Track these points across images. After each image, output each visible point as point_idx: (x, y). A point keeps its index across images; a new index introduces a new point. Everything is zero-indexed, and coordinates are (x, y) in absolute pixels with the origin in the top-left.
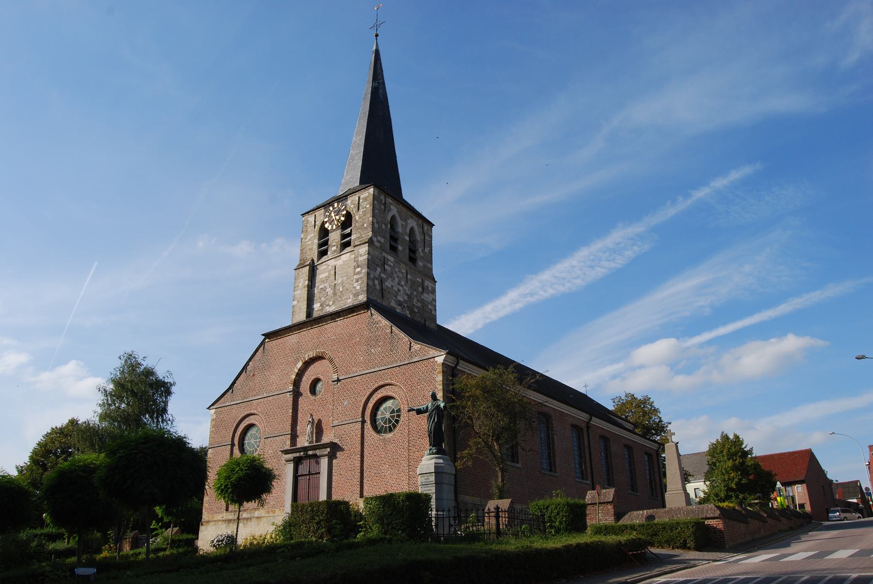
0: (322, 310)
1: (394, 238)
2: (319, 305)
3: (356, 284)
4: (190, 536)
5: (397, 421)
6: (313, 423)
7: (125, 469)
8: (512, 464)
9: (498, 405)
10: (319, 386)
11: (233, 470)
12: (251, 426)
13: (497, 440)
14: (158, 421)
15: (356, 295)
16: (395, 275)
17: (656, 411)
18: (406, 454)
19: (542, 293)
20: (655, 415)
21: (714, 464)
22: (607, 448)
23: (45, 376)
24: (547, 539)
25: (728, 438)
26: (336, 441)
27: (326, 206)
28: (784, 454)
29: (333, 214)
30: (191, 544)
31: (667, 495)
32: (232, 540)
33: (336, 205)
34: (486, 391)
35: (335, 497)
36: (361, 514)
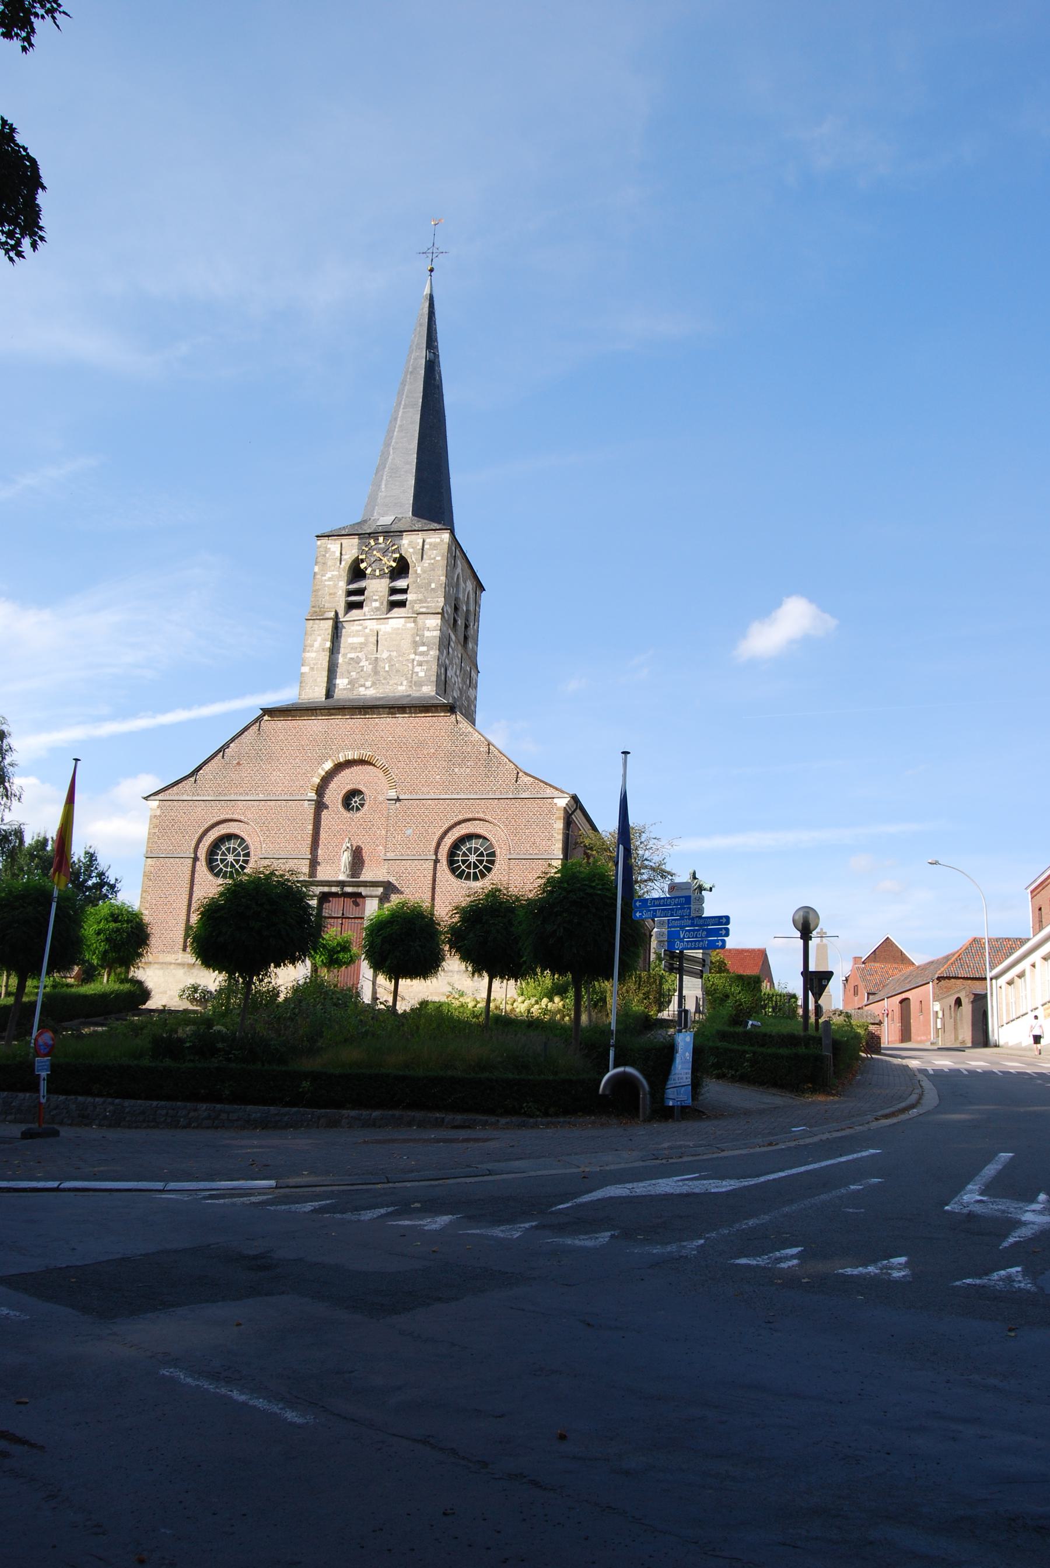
2: (346, 681)
3: (417, 669)
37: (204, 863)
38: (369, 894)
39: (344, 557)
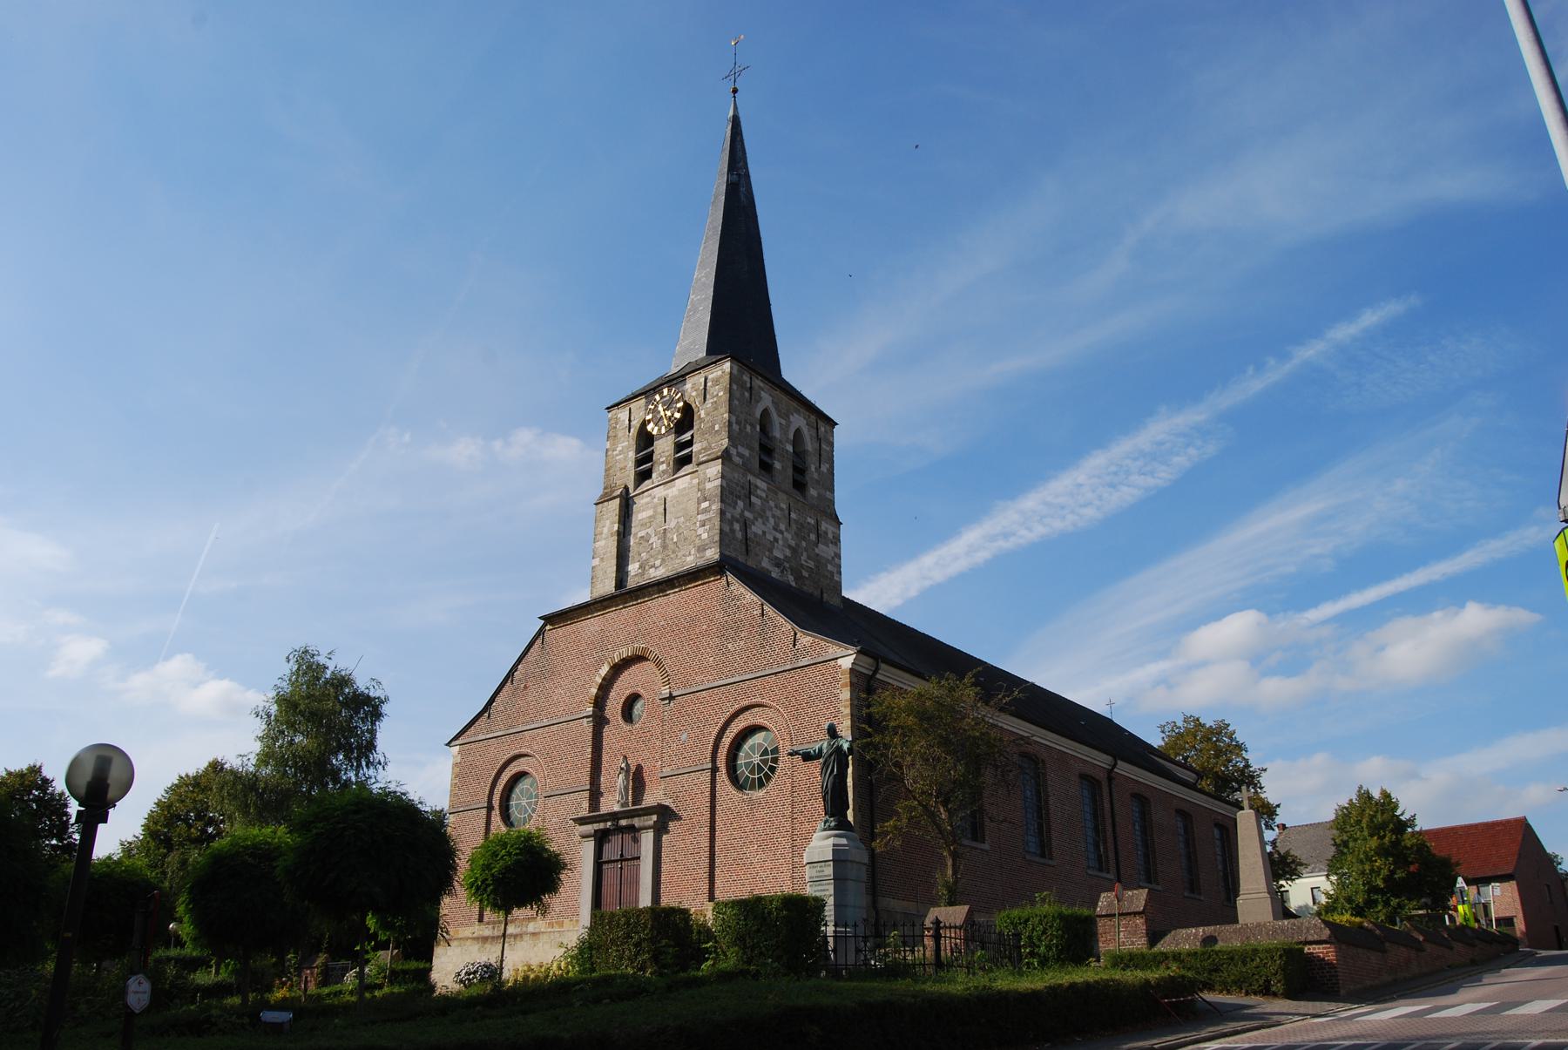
0: (642, 574)
1: (767, 449)
2: (637, 565)
3: (700, 531)
4: (422, 965)
5: (772, 769)
6: (628, 771)
7: (315, 845)
8: (975, 844)
9: (945, 742)
10: (638, 707)
11: (495, 854)
12: (520, 776)
13: (945, 804)
14: (359, 765)
15: (701, 549)
16: (769, 514)
17: (1240, 747)
18: (788, 826)
19: (1023, 532)
20: (1238, 755)
21: (1345, 844)
22: (1145, 815)
23: (139, 680)
24: (1021, 974)
25: (1370, 798)
26: (668, 802)
27: (648, 392)
28: (1476, 826)
29: (660, 408)
30: (423, 976)
31: (1240, 901)
32: (492, 973)
33: (665, 391)
34: (923, 716)
35: (665, 901)
36: (709, 930)
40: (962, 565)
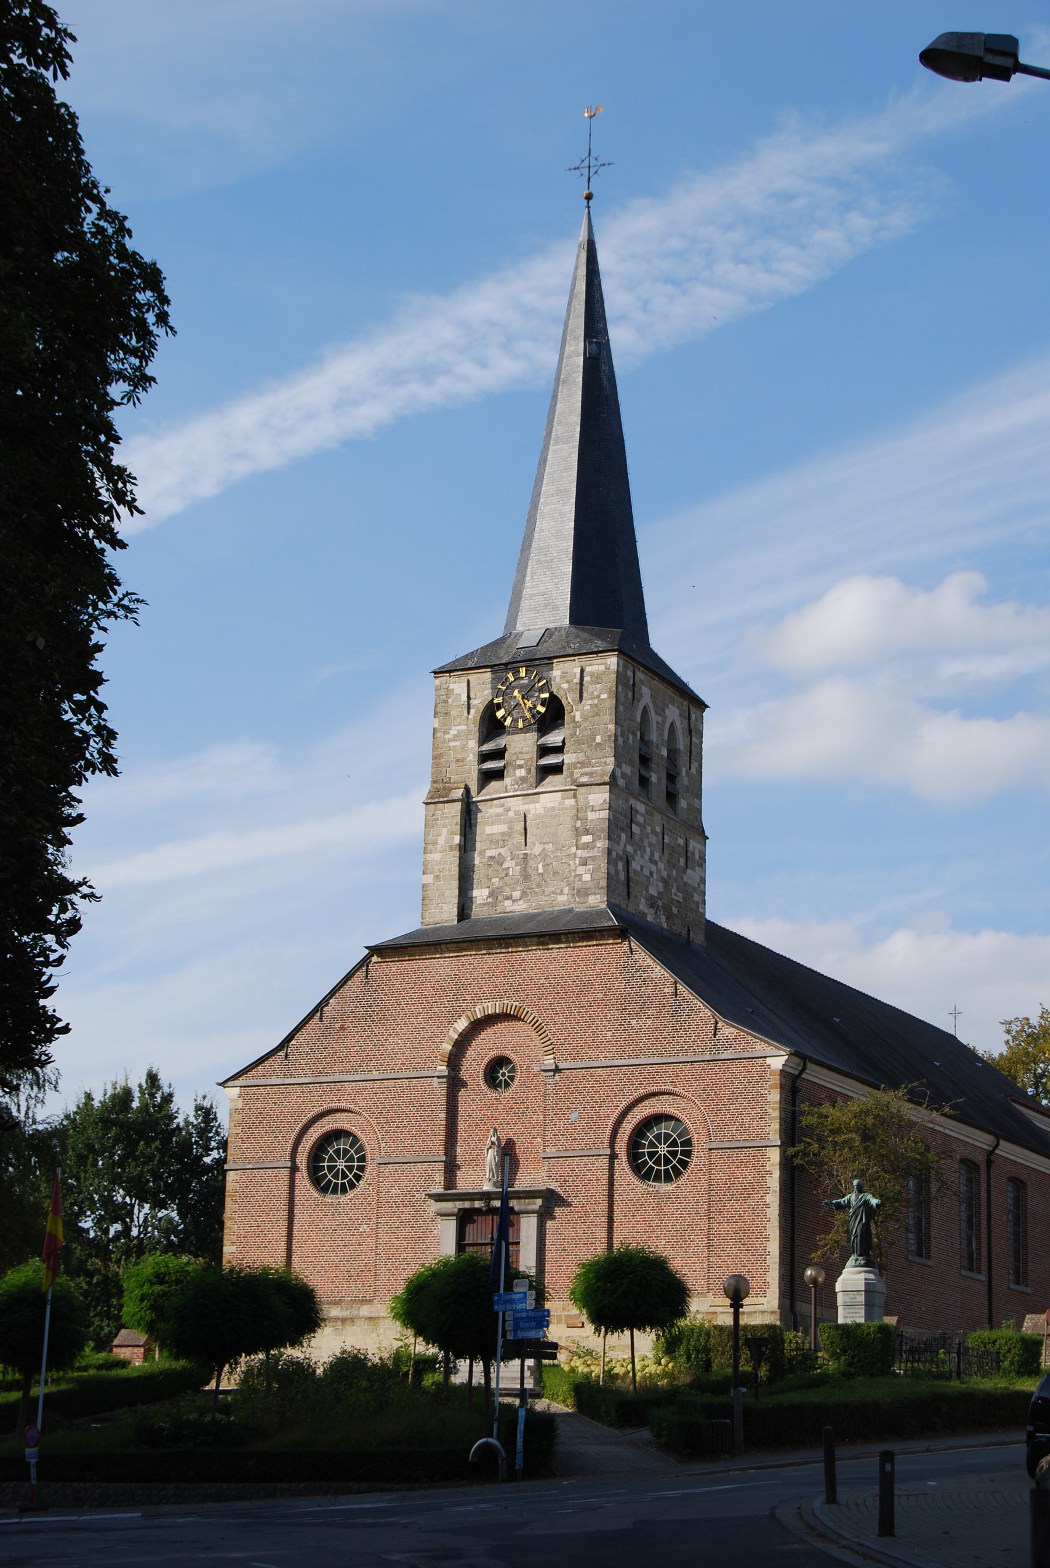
2: (485, 892)
3: (581, 870)
16: (646, 843)
37: (305, 1174)
38: (523, 1208)
39: (473, 702)
40: (325, 431)
